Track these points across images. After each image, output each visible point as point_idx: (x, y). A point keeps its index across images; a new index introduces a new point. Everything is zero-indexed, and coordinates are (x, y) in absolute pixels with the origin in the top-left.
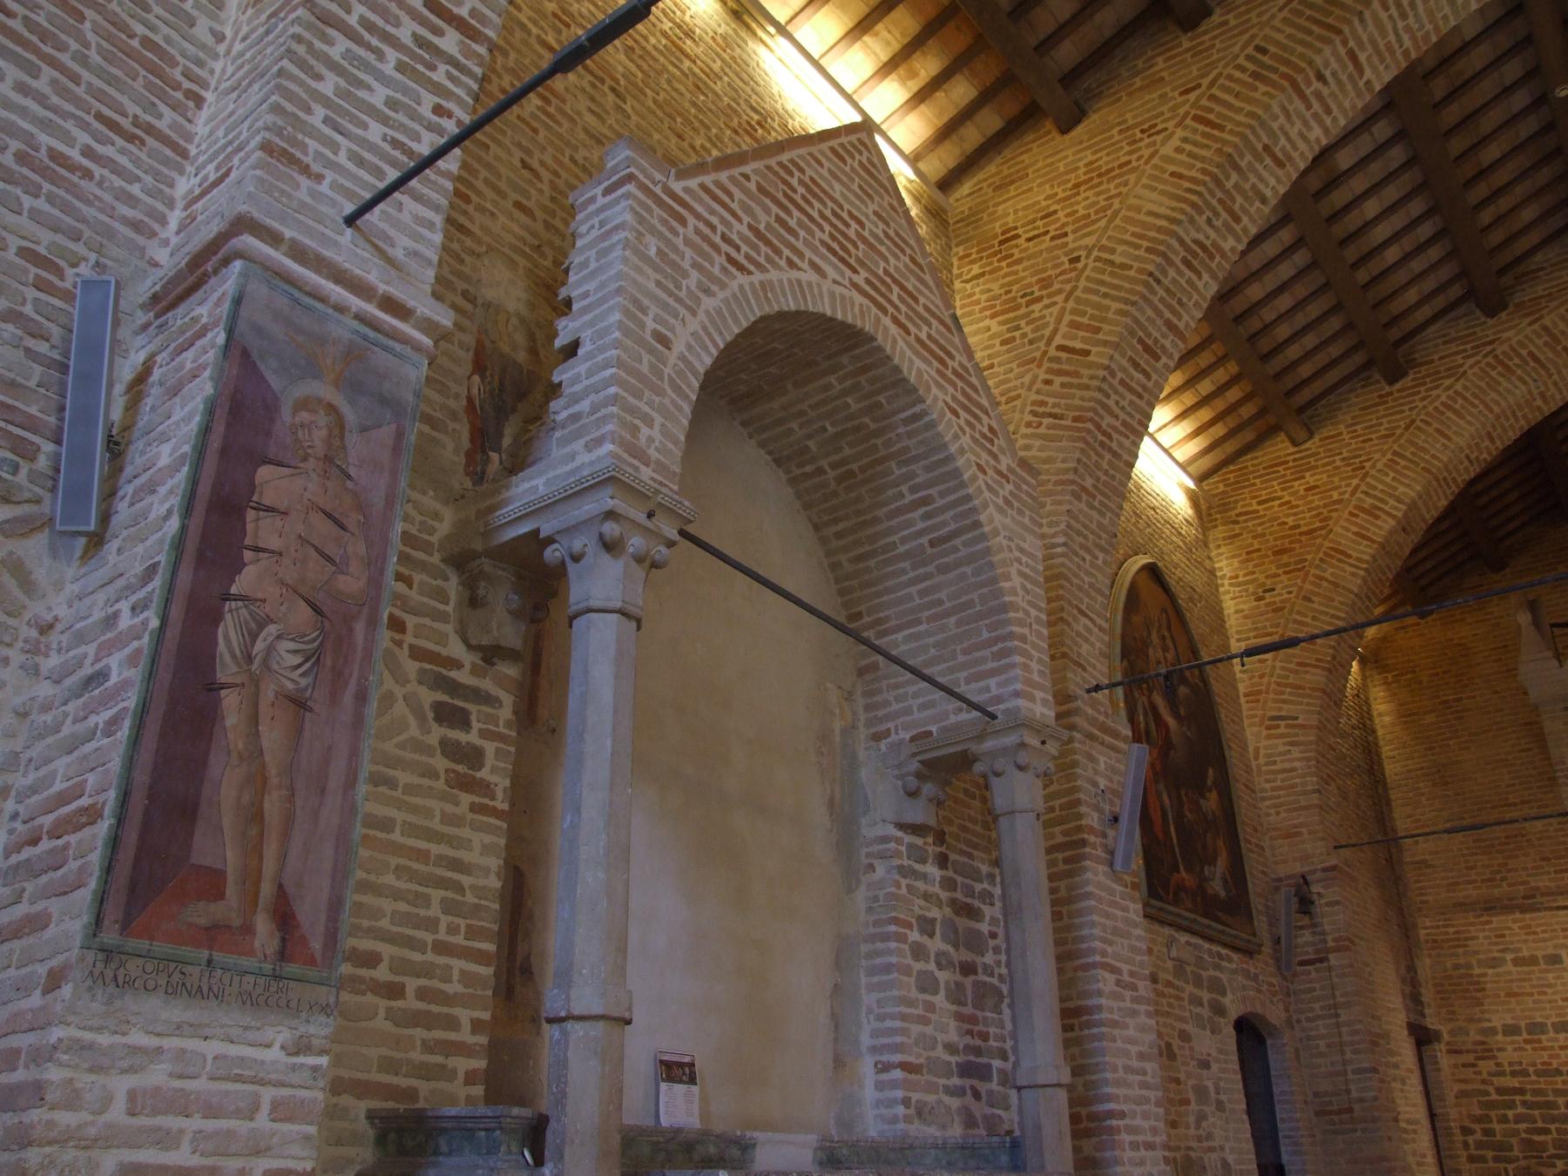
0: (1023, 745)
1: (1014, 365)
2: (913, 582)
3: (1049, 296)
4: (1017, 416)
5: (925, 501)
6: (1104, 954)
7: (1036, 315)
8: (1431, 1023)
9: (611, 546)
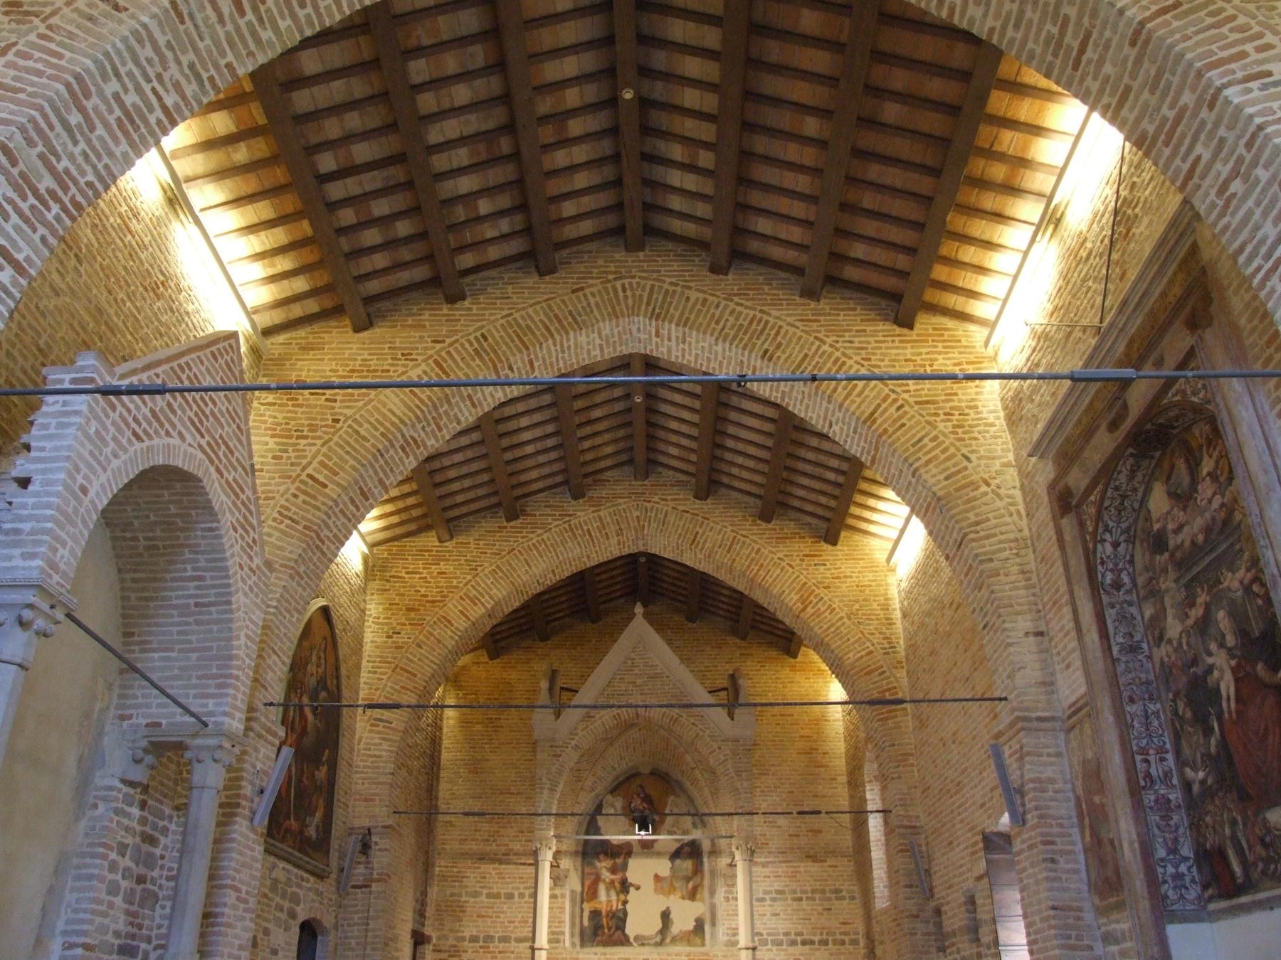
0: (221, 747)
1: (277, 475)
2: (178, 624)
3: (313, 438)
4: (269, 510)
5: (200, 578)
6: (234, 879)
7: (301, 447)
8: (428, 931)
9: (23, 624)
